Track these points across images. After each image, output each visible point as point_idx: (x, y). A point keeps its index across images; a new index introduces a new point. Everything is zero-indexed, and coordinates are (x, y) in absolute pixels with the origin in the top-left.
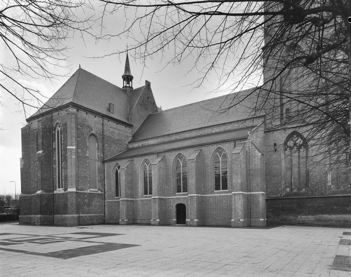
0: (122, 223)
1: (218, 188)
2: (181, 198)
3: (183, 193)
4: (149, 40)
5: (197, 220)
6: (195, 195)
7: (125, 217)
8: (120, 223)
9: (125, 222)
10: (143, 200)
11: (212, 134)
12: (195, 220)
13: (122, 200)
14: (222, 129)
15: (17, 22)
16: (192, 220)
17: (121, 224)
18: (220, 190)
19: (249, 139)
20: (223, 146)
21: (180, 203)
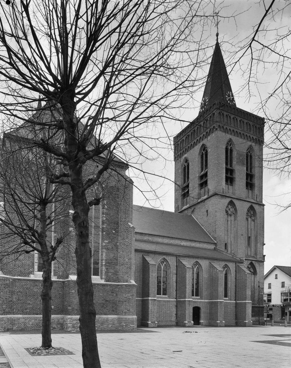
0: (153, 325)
1: (159, 293)
2: (197, 302)
3: (196, 297)
4: (19, 90)
5: (217, 322)
6: (187, 299)
7: (154, 319)
8: (187, 325)
9: (156, 325)
10: (160, 301)
11: (157, 243)
12: (219, 322)
13: (152, 300)
14: (166, 241)
15: (92, 28)
16: (221, 322)
17: (151, 326)
18: (161, 295)
19: (244, 264)
20: (168, 258)
21: (197, 306)
